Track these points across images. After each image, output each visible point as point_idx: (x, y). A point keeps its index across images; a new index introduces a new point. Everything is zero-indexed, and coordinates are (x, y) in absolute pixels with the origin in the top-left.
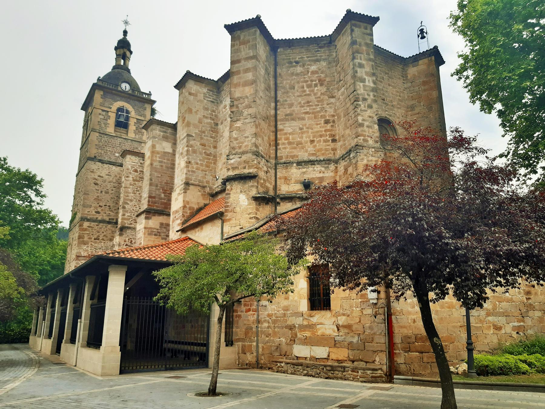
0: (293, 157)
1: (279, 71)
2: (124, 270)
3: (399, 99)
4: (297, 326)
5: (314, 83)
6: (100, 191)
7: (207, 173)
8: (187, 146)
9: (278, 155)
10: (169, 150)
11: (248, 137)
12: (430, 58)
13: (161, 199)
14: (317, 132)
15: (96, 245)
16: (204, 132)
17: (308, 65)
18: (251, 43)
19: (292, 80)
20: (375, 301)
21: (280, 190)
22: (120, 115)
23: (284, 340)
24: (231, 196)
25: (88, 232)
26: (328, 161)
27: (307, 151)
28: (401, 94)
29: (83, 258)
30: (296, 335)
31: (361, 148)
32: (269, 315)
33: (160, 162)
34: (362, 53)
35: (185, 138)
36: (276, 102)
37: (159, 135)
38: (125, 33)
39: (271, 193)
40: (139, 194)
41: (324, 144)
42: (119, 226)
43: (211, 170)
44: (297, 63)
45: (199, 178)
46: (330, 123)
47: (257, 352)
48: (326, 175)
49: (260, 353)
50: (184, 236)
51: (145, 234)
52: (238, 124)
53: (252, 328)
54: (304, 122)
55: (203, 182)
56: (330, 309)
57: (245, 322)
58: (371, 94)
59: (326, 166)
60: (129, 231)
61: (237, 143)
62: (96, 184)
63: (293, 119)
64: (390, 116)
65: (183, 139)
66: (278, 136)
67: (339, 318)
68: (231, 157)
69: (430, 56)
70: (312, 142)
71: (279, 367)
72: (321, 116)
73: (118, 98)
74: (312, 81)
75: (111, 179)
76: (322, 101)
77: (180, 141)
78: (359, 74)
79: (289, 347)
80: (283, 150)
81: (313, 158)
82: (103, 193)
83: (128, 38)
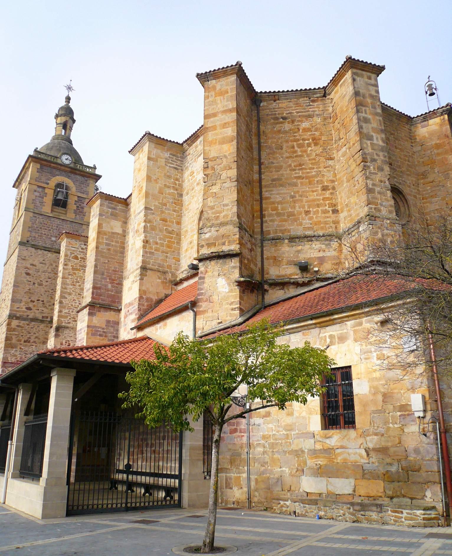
0: (283, 232)
1: (262, 128)
2: (73, 373)
3: (408, 164)
4: (306, 451)
5: (307, 142)
6: (32, 283)
7: (168, 255)
8: (145, 221)
9: (265, 229)
10: (119, 230)
11: (227, 205)
12: (442, 117)
13: (108, 291)
14: (314, 200)
15: (27, 349)
16: (165, 205)
17: (298, 121)
18: (230, 94)
19: (279, 138)
20: (421, 414)
21: (268, 274)
22: (59, 191)
23: (287, 470)
24: (207, 280)
25: (16, 333)
26: (329, 237)
27: (301, 224)
28: (410, 159)
29: (10, 365)
30: (305, 463)
31: (373, 218)
32: (264, 437)
33: (108, 245)
34: (367, 107)
35: (141, 211)
36: (260, 164)
37: (107, 213)
38: (68, 99)
39: (258, 278)
40: (80, 286)
41: (323, 215)
42: (55, 325)
43: (173, 252)
44: (284, 118)
45: (159, 262)
46: (329, 190)
47: (249, 487)
48: (327, 254)
49: (252, 487)
50: (140, 334)
51: (88, 334)
52: (215, 189)
53: (240, 455)
54: (296, 189)
55: (163, 266)
56: (354, 427)
57: (230, 447)
58: (381, 154)
59: (327, 242)
60: (66, 332)
61: (213, 213)
62: (28, 274)
63: (282, 185)
64: (400, 184)
65: (139, 213)
66: (264, 206)
67: (368, 438)
68: (205, 230)
69: (442, 114)
70: (307, 212)
71: (282, 506)
72: (317, 181)
73: (57, 173)
74: (304, 140)
75: (46, 269)
76: (317, 163)
77: (135, 216)
78: (365, 131)
79: (295, 479)
80: (270, 223)
81: (309, 233)
82: (36, 285)
83: (71, 105)
